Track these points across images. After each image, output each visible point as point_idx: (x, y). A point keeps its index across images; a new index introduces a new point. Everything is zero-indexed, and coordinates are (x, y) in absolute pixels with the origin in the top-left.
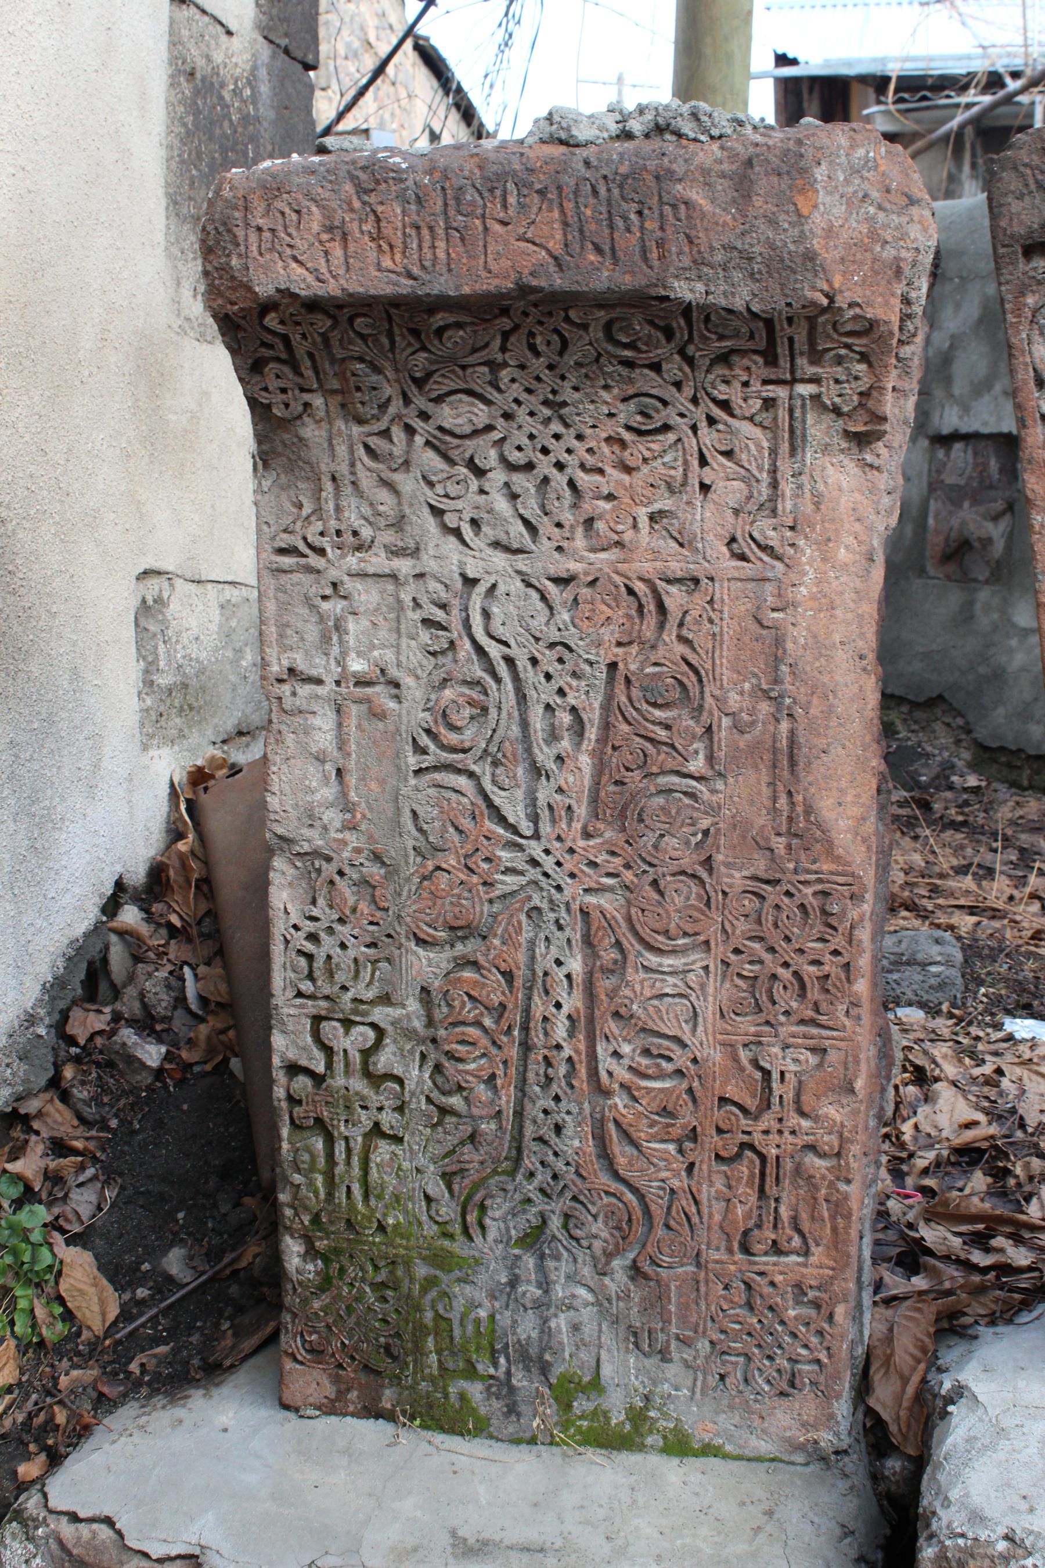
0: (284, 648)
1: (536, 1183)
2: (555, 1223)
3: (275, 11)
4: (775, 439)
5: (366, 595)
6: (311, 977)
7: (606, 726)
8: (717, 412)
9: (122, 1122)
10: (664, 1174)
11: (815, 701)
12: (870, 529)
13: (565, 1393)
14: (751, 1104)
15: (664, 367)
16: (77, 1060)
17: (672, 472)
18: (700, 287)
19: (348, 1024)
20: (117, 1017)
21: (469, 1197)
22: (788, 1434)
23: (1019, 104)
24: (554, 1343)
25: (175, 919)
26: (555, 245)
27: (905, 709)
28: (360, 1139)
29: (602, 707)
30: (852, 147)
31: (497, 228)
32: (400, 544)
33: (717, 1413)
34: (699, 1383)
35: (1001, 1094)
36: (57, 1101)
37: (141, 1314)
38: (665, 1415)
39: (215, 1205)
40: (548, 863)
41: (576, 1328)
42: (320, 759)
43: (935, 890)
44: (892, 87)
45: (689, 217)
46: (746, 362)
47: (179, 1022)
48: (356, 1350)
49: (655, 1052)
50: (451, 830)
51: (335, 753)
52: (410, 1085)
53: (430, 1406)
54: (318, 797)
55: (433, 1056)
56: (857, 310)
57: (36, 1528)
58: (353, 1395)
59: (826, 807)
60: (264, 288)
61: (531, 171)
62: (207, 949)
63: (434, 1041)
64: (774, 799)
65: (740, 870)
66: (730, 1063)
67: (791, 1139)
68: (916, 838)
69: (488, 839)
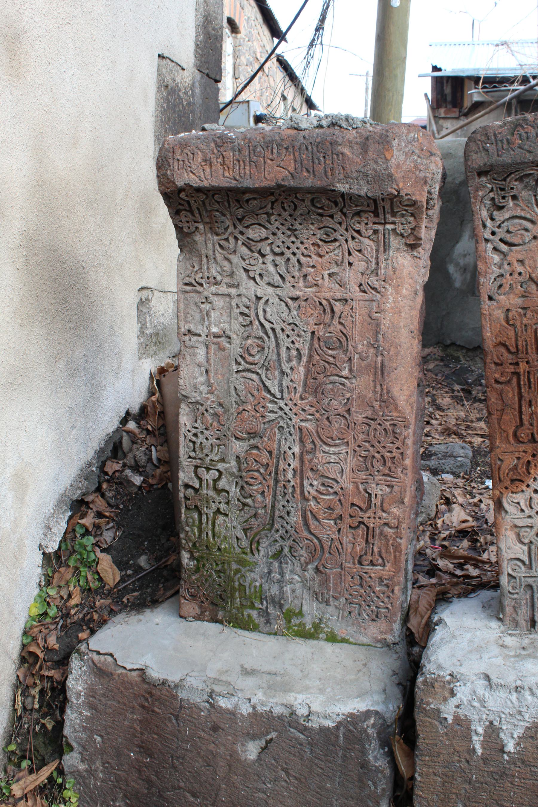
0: (187, 322)
1: (279, 534)
2: (286, 550)
3: (203, 59)
4: (378, 246)
5: (219, 302)
6: (194, 450)
7: (310, 356)
8: (355, 235)
9: (125, 506)
10: (329, 533)
11: (392, 349)
12: (416, 282)
13: (289, 616)
14: (364, 506)
15: (335, 216)
16: (108, 481)
17: (338, 258)
18: (347, 186)
19: (208, 469)
20: (124, 465)
21: (253, 538)
22: (375, 636)
23: (535, 90)
24: (285, 596)
25: (149, 427)
26: (291, 169)
27: (464, 351)
28: (212, 514)
29: (309, 349)
30: (408, 133)
31: (269, 162)
32: (232, 283)
33: (347, 626)
34: (341, 615)
35: (480, 510)
36: (100, 497)
37: (129, 580)
38: (327, 626)
39: (159, 540)
40: (287, 409)
41: (293, 591)
42: (200, 365)
43: (468, 427)
44: (481, 81)
45: (343, 159)
46: (366, 215)
48: (208, 596)
49: (326, 484)
50: (249, 395)
51: (205, 364)
52: (231, 494)
53: (237, 619)
54: (198, 380)
55: (240, 483)
56: (409, 197)
57: (84, 656)
58: (207, 613)
59: (396, 391)
60: (180, 183)
61: (282, 140)
63: (241, 477)
64: (375, 387)
65: (361, 414)
66: (355, 490)
67: (379, 521)
68: (463, 405)
69: (263, 399)
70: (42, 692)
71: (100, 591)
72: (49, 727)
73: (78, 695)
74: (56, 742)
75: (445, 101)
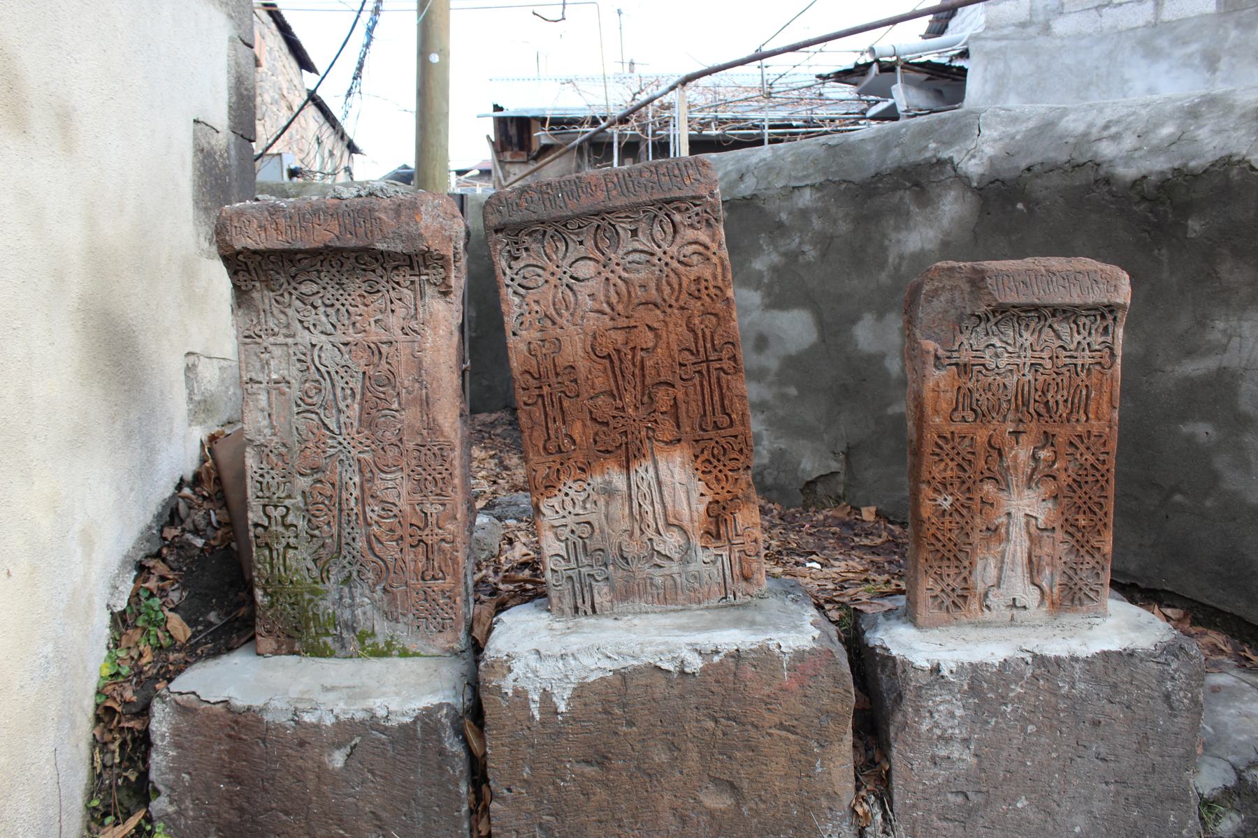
2: (355, 574)
5: (277, 351)
7: (363, 394)
13: (362, 637)
14: (422, 525)
16: (168, 546)
19: (276, 507)
20: (183, 530)
26: (337, 232)
40: (345, 443)
42: (262, 410)
47: (209, 532)
59: (440, 419)
60: (238, 247)
62: (220, 504)
70: (123, 745)
71: (173, 648)
72: (133, 778)
73: (163, 736)
74: (143, 791)
75: (510, 143)
